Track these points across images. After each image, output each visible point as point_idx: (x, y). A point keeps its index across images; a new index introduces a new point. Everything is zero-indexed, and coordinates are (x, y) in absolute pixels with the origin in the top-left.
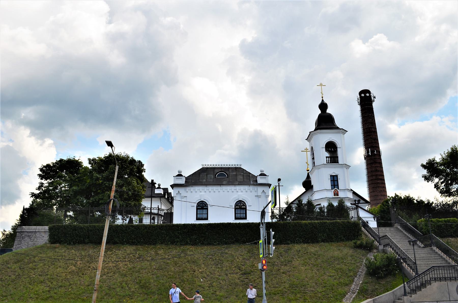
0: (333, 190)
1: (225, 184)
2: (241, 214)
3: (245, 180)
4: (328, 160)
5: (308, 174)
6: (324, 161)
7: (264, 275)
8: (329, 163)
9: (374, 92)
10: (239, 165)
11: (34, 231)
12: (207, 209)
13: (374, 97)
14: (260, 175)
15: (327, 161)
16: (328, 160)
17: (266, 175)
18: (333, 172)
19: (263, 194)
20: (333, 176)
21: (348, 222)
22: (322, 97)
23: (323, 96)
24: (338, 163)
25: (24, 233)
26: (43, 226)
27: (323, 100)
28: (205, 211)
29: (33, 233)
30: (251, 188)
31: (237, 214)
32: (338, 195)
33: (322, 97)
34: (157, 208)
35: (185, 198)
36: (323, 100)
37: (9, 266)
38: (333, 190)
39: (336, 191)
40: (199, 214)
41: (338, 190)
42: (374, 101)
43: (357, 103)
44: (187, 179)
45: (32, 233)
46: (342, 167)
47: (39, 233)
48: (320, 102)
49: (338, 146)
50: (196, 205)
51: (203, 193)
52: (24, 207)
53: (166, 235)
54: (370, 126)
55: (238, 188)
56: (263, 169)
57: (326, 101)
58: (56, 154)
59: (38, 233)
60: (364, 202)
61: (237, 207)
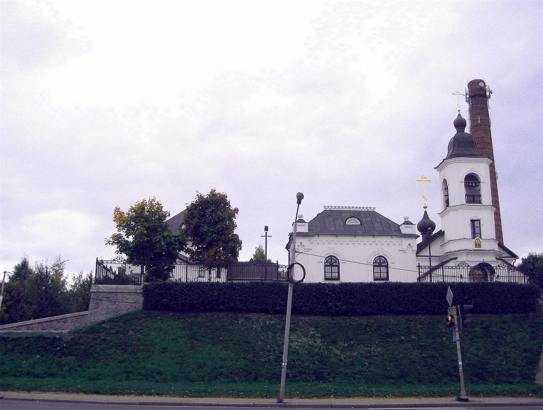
1: (360, 234)
3: (385, 229)
5: (426, 212)
6: (463, 200)
7: (284, 347)
9: (490, 84)
10: (372, 209)
11: (115, 291)
12: (338, 266)
13: (491, 92)
14: (404, 224)
17: (412, 224)
18: (474, 215)
19: (410, 248)
22: (459, 111)
24: (480, 202)
25: (101, 293)
26: (126, 284)
27: (459, 115)
28: (335, 269)
29: (113, 293)
30: (395, 240)
32: (480, 246)
33: (459, 111)
35: (310, 251)
36: (459, 115)
41: (481, 240)
42: (489, 97)
43: (465, 100)
44: (311, 224)
45: (111, 293)
47: (121, 294)
48: (455, 117)
49: (481, 181)
50: (323, 260)
51: (333, 245)
52: (97, 259)
54: (483, 134)
55: (378, 239)
56: (406, 215)
59: (120, 294)
60: (509, 255)
61: (376, 264)
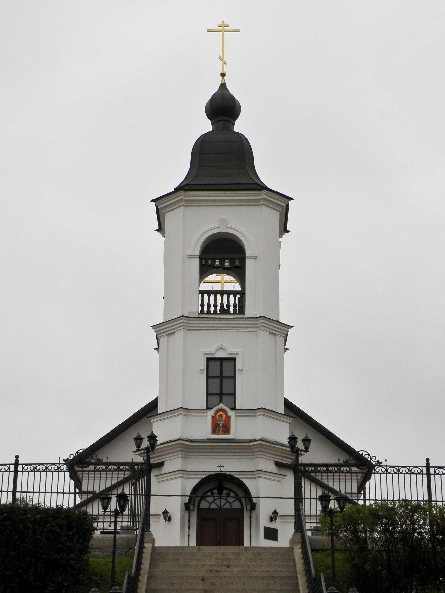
0: (211, 413)
2: (54, 495)
4: (206, 302)
8: (204, 313)
15: (203, 305)
16: (206, 302)
18: (218, 345)
20: (221, 360)
21: (371, 510)
22: (223, 75)
23: (226, 71)
27: (223, 86)
31: (356, 474)
32: (227, 430)
33: (223, 75)
34: (12, 468)
36: (223, 86)
37: (252, 585)
38: (211, 413)
39: (221, 416)
40: (8, 492)
41: (231, 413)
46: (254, 329)
53: (361, 518)
57: (233, 89)
58: (219, 309)
